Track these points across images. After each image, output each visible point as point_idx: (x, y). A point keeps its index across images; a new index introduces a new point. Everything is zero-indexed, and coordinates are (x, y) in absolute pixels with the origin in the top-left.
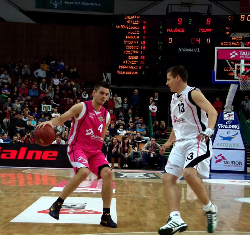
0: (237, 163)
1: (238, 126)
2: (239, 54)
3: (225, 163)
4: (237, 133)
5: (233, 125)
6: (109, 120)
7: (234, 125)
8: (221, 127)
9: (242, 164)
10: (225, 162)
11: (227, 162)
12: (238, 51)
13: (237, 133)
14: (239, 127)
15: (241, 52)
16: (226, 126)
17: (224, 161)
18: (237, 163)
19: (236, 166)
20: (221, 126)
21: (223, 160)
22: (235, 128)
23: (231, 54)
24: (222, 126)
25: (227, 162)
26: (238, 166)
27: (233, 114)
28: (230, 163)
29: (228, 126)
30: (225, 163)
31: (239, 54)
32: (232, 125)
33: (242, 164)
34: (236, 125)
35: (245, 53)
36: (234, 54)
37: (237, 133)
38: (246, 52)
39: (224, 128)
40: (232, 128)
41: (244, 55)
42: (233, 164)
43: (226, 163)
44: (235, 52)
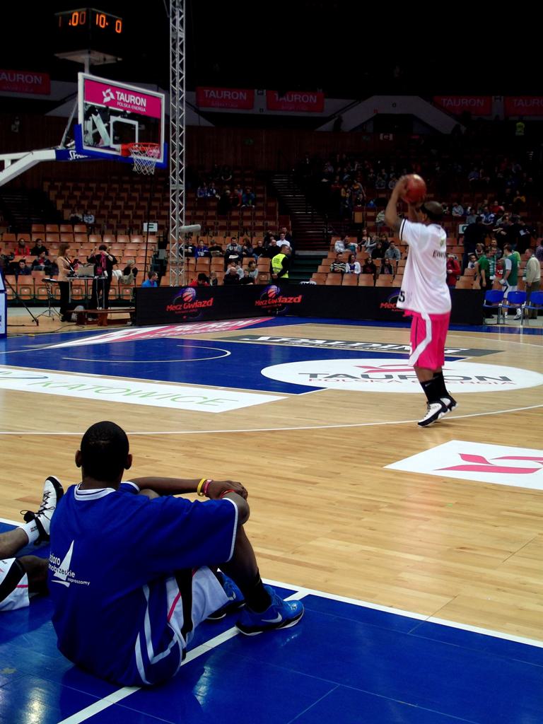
2: (115, 95)
6: (35, 161)
15: (118, 93)
23: (104, 94)
31: (115, 95)
36: (108, 95)
38: (126, 95)
41: (122, 101)
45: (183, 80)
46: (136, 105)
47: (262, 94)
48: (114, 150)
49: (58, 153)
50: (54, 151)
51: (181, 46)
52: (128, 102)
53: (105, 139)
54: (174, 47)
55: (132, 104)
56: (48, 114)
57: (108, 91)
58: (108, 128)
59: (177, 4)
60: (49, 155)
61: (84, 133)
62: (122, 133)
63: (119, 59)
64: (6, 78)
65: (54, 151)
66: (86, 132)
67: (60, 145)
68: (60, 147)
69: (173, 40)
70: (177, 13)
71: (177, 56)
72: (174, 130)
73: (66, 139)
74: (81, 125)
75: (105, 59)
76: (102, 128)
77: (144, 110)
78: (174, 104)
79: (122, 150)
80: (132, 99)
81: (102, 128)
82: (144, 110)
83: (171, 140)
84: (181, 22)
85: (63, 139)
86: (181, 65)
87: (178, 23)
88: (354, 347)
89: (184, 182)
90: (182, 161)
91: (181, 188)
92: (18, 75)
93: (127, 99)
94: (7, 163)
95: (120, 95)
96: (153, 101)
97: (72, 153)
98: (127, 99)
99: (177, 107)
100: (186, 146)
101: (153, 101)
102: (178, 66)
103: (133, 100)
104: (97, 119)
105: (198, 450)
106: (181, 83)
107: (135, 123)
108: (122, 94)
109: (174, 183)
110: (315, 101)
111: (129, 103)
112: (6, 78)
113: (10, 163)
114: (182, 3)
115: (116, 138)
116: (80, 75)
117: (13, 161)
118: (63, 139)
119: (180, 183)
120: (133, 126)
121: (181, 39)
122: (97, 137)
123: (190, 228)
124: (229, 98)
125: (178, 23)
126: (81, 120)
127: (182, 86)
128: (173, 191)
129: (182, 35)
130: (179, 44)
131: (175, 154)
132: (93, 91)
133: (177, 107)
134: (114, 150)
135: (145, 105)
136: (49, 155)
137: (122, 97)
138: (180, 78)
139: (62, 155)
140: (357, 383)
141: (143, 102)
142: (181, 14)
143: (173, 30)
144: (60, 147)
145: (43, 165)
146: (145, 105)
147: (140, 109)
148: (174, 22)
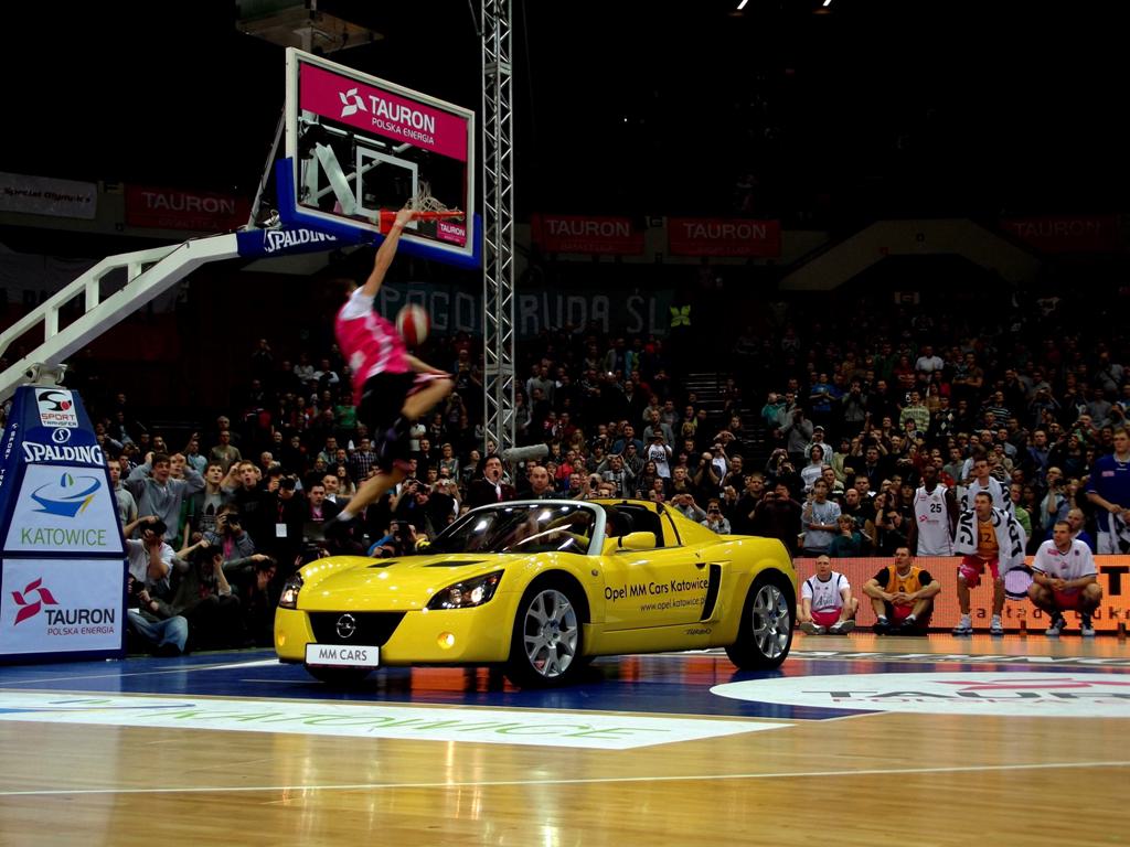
0: (97, 616)
1: (96, 451)
2: (368, 103)
3: (53, 619)
4: (98, 485)
5: (78, 446)
7: (82, 448)
8: (278, 242)
9: (112, 621)
10: (54, 615)
11: (60, 617)
12: (366, 90)
13: (94, 482)
14: (100, 455)
15: (375, 99)
16: (291, 235)
17: (50, 612)
18: (97, 616)
19: (92, 631)
20: (277, 237)
21: (45, 607)
22: (89, 461)
24: (281, 238)
25: (60, 612)
26: (99, 630)
27: (70, 402)
28: (71, 620)
29: (298, 237)
30: (53, 619)
31: (368, 103)
32: (76, 448)
33: (112, 621)
34: (88, 448)
35: (706, 231)
36: (352, 101)
37: (98, 485)
38: (293, 232)
39: (285, 245)
40: (78, 459)
42: (83, 620)
43: (57, 620)
44: (342, 95)
45: (508, 155)
46: (412, 128)
47: (661, 225)
48: (365, 220)
49: (242, 239)
50: (233, 237)
51: (505, 90)
52: (396, 119)
53: (346, 200)
54: (491, 92)
55: (405, 125)
56: (243, 269)
57: (352, 92)
58: (352, 184)
59: (496, 9)
60: (224, 246)
61: (300, 193)
62: (385, 189)
63: (378, 37)
64: (165, 203)
65: (235, 235)
66: (304, 191)
67: (246, 223)
68: (248, 228)
69: (488, 80)
70: (497, 26)
71: (497, 109)
72: (491, 185)
73: (261, 207)
74: (291, 158)
75: (346, 37)
76: (339, 180)
77: (431, 141)
78: (488, 133)
79: (382, 221)
80: (404, 114)
81: (339, 180)
82: (431, 141)
83: (486, 275)
84: (504, 44)
85: (255, 209)
86: (505, 127)
87: (498, 47)
88: (908, 659)
89: (513, 360)
90: (509, 282)
91: (508, 372)
92: (189, 198)
93: (394, 115)
94: (134, 271)
95: (378, 104)
96: (447, 122)
97: (273, 236)
98: (394, 115)
99: (498, 246)
100: (515, 250)
101: (447, 122)
102: (498, 130)
103: (408, 117)
104: (324, 152)
105: (579, 813)
106: (506, 199)
107: (413, 167)
108: (383, 103)
109: (491, 361)
110: (763, 236)
111: (398, 123)
112: (165, 203)
113: (139, 271)
114: (505, 6)
115: (368, 197)
116: (292, 55)
117: (146, 267)
118: (255, 209)
119: (505, 361)
120: (410, 172)
121: (504, 77)
122: (329, 202)
123: (525, 452)
124: (597, 233)
125: (498, 47)
126: (291, 150)
127: (491, 324)
128: (491, 378)
129: (505, 68)
130: (500, 86)
131: (493, 195)
132: (316, 89)
133: (498, 246)
134: (365, 220)
135: (432, 131)
136: (224, 246)
137: (383, 108)
138: (503, 153)
139: (252, 245)
140: (955, 704)
141: (428, 123)
142: (504, 29)
143: (487, 61)
144: (248, 228)
145: (209, 271)
146: (432, 131)
147: (421, 136)
148: (490, 45)
